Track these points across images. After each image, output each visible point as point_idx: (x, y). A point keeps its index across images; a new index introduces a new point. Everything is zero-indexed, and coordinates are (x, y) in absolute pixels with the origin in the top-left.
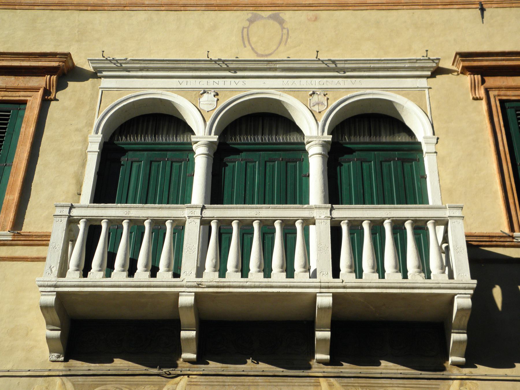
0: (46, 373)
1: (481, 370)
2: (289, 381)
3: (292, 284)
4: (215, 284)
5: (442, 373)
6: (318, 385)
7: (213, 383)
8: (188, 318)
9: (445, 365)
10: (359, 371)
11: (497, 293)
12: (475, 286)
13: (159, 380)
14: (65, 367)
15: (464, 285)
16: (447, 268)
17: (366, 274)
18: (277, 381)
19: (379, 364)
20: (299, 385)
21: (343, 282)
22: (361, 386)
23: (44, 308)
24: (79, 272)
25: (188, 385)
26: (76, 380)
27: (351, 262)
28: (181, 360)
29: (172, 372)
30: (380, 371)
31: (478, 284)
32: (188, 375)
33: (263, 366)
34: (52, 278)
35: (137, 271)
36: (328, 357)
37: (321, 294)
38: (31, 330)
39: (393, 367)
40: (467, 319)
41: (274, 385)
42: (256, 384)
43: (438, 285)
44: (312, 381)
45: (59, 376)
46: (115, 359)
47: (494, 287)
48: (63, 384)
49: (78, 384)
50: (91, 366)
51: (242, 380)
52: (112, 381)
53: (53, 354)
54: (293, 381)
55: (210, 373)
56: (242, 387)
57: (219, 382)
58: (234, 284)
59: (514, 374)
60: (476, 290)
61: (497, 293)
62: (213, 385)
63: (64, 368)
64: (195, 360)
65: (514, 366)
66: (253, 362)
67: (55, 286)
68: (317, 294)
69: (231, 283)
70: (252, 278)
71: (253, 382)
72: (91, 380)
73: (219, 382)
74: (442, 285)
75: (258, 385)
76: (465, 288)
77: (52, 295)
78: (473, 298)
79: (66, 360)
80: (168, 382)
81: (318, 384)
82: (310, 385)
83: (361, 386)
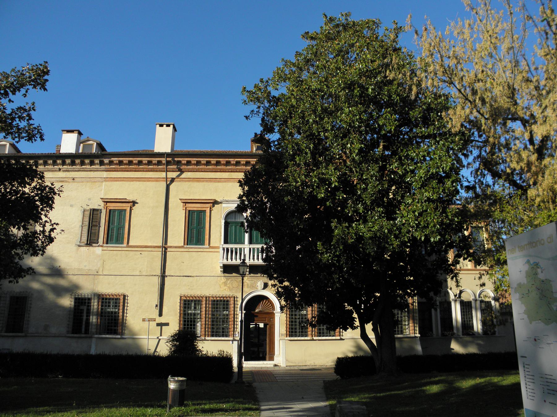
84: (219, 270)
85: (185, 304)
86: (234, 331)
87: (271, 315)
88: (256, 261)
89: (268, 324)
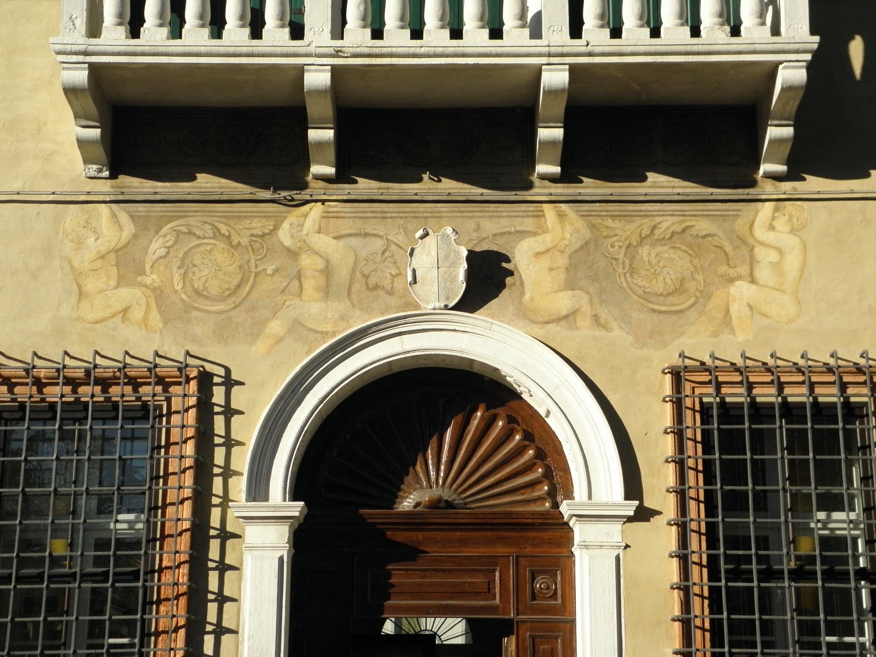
0: (83, 198)
1: (813, 184)
2: (492, 209)
3: (499, 50)
4: (366, 51)
5: (747, 191)
6: (541, 215)
7: (365, 215)
8: (320, 108)
10: (609, 191)
11: (856, 49)
12: (816, 46)
13: (275, 209)
14: (112, 187)
15: (797, 46)
16: (771, 8)
17: (628, 30)
18: (474, 209)
19: (644, 179)
20: (509, 217)
21: (588, 45)
22: (611, 216)
23: (71, 92)
24: (123, 28)
26: (135, 209)
27: (604, 7)
28: (311, 176)
29: (295, 197)
30: (644, 191)
31: (821, 44)
32: (323, 202)
33: (449, 186)
34: (78, 38)
35: (227, 27)
36: (557, 169)
37: (549, 67)
38: (45, 124)
39: (665, 184)
40: (797, 103)
41: (467, 217)
42: (436, 215)
43: (751, 47)
44: (531, 209)
46: (197, 175)
47: (853, 38)
48: (114, 215)
49: (139, 216)
50: (157, 187)
51: (414, 210)
52: (196, 211)
53: (90, 166)
54: (499, 209)
55: (360, 197)
56: (413, 220)
57: (375, 212)
58: (399, 50)
59: (865, 188)
60: (816, 54)
61: (856, 49)
62: (365, 218)
63: (111, 190)
64: (334, 177)
65: (868, 175)
66: (431, 178)
67: (86, 53)
68: (543, 67)
69: (394, 50)
70: (429, 39)
71: (433, 212)
72: (159, 209)
73: (375, 212)
74: (759, 47)
75: (441, 217)
76: (797, 52)
77: (81, 69)
78: (811, 67)
79: (113, 176)
80: (290, 212)
81: (541, 213)
82: (528, 216)
83: (611, 216)
84: (64, 141)
85: (731, 442)
87: (543, 541)
89: (507, 627)
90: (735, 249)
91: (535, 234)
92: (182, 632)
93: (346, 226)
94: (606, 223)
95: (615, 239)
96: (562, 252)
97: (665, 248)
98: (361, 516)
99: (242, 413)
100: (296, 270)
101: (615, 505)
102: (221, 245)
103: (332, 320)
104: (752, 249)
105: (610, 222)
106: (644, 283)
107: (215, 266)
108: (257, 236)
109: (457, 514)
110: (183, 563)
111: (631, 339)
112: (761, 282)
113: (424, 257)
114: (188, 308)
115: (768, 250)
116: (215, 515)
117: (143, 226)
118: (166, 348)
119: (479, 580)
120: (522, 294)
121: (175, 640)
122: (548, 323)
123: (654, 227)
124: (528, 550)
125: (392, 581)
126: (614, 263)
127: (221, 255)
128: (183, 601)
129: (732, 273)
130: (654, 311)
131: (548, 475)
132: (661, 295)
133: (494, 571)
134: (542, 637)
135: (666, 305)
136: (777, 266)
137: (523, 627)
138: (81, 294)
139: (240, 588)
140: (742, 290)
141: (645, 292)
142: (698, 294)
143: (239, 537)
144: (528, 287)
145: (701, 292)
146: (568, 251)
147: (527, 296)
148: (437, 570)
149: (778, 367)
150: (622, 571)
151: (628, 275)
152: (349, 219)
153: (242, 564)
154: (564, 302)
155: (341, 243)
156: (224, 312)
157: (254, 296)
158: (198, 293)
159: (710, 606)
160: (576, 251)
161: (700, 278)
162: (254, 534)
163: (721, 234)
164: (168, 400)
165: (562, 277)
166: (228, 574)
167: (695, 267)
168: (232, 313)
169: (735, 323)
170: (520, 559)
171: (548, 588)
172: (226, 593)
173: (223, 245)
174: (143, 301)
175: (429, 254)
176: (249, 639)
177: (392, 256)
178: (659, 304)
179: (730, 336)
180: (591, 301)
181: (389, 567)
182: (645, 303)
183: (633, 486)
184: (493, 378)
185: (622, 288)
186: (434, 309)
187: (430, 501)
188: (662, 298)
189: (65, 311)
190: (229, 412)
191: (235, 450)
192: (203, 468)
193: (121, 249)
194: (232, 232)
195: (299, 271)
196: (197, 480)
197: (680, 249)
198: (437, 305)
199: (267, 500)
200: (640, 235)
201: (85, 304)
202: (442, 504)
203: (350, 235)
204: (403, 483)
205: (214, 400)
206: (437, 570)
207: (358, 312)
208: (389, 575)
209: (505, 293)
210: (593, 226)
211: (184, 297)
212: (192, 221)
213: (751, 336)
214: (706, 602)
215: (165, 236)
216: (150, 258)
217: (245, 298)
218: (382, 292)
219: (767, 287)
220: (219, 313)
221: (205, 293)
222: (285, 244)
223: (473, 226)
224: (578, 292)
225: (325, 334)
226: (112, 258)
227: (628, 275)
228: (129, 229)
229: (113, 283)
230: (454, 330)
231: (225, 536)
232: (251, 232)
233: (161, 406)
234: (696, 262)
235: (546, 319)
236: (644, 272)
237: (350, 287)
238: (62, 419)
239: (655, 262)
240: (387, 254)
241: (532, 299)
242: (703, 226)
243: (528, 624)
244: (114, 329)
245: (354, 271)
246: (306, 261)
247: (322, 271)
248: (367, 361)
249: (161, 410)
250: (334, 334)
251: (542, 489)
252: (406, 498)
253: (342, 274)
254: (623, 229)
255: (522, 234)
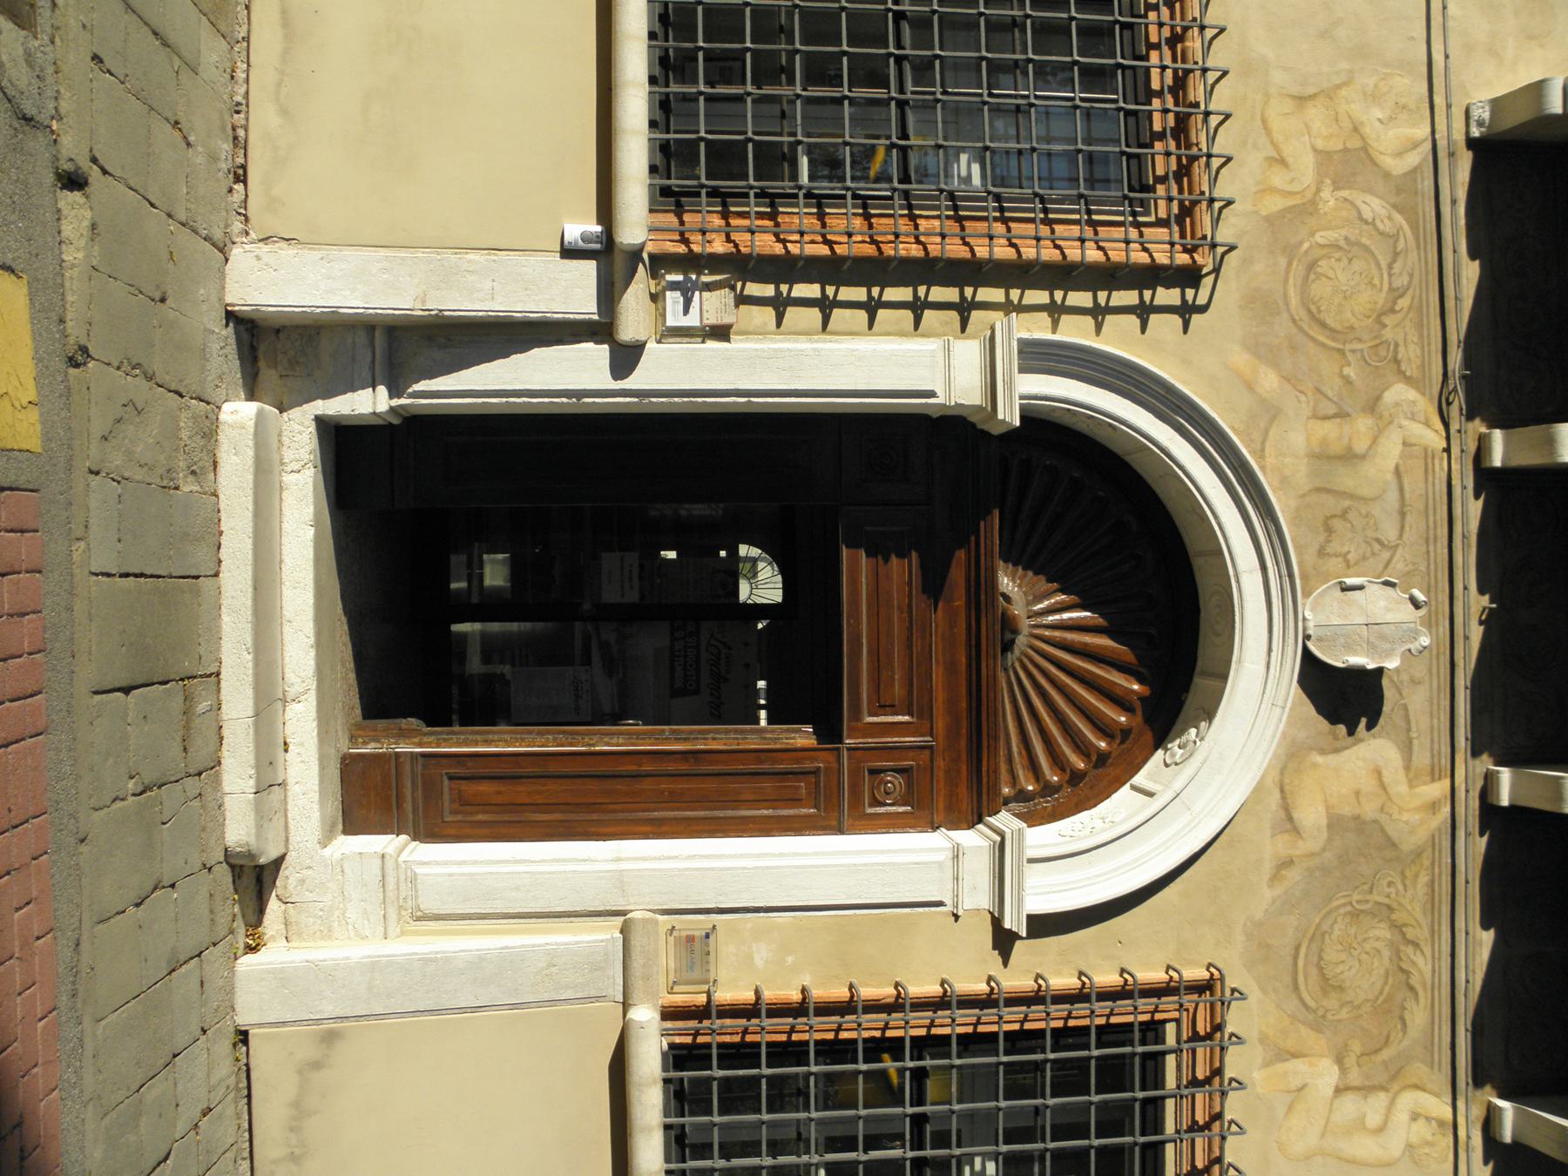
0: (1439, 100)
6: (1434, 776)
7: (1431, 512)
9: (1488, 1088)
19: (1485, 926)
20: (1432, 728)
22: (1432, 881)
25: (1426, 450)
28: (1483, 430)
29: (1455, 409)
32: (1448, 450)
36: (1505, 801)
38: (1541, 46)
45: (1433, 132)
46: (1477, 263)
53: (1487, 108)
62: (1427, 512)
64: (1486, 464)
79: (1471, 143)
80: (1431, 399)
83: (1432, 881)
86: (741, 267)
88: (1027, 622)
90: (1385, 1064)
91: (1407, 768)
92: (824, 250)
93: (1414, 484)
94: (1423, 873)
95: (1400, 887)
96: (1382, 809)
97: (1386, 961)
98: (989, 512)
99: (1143, 330)
100: (1350, 410)
101: (1020, 901)
102: (1381, 299)
103: (1282, 465)
104: (1383, 1088)
105: (1424, 879)
106: (1337, 932)
107: (1349, 290)
108: (1396, 352)
109: (995, 657)
110: (925, 249)
111: (1259, 915)
112: (1338, 1101)
113: (1382, 603)
114: (1290, 251)
115: (1383, 1111)
116: (994, 294)
117: (1402, 186)
118: (1232, 220)
119: (898, 690)
120: (1323, 752)
121: (813, 242)
122: (1282, 791)
123: (1416, 945)
124: (940, 763)
125: (894, 560)
126: (1366, 887)
127: (1367, 299)
128: (870, 250)
129: (1351, 1060)
130: (1297, 948)
131: (1047, 789)
132: (1320, 958)
133: (910, 714)
134: (817, 784)
135: (1305, 965)
136: (1359, 1124)
137: (831, 757)
138: (1301, 100)
139: (889, 334)
140: (1325, 1075)
141: (1323, 935)
142: (1320, 1013)
143: (963, 329)
144: (1333, 760)
145: (1323, 1017)
146: (1383, 818)
147: (1319, 759)
148: (910, 629)
149: (1223, 1138)
150: (921, 910)
151: (1349, 908)
152: (1424, 488)
153: (923, 336)
154: (1311, 815)
155: (1390, 477)
156: (1287, 305)
157: (1312, 348)
158: (1311, 266)
159: (873, 1039)
160: (1383, 830)
161: (1344, 1014)
162: (968, 352)
163: (1406, 1043)
164: (1160, 223)
165: (1347, 810)
166: (908, 315)
167: (1359, 1007)
168: (1285, 315)
169: (1280, 1067)
170: (927, 752)
171: (887, 794)
172: (881, 313)
173: (1381, 302)
174: (1297, 187)
175: (1388, 610)
176: (815, 350)
177: (1373, 554)
178: (1306, 956)
179: (1259, 1061)
180: (1312, 854)
181: (914, 554)
182: (1309, 935)
183: (1044, 926)
184: (1185, 708)
185: (1330, 900)
186: (1304, 619)
187: (1015, 617)
188: (1315, 959)
189: (1277, 77)
190: (1143, 312)
191: (1089, 321)
192: (1064, 275)
193: (1368, 155)
194: (1399, 316)
195: (1348, 415)
196: (1048, 267)
197: (1386, 983)
198: (1311, 624)
199: (1022, 370)
200: (1405, 925)
201: (1288, 106)
202: (1008, 636)
203: (1401, 489)
204: (1036, 573)
205: (1160, 290)
206: (910, 629)
207: (1293, 503)
208: (902, 555)
209: (1323, 724)
210: (1419, 855)
211: (1306, 245)
212: (1413, 256)
213: (1259, 1090)
214: (877, 1034)
215: (1390, 218)
216: (1358, 198)
217: (1308, 336)
218: (1322, 539)
219: (1330, 1111)
220: (1285, 295)
221: (1312, 276)
222: (1386, 394)
223: (1418, 675)
224: (1325, 835)
225: (1260, 454)
226: (1355, 143)
227: (1349, 908)
228: (1398, 166)
229: (1320, 144)
230: (1270, 650)
231: (964, 309)
232: (1401, 343)
233: (1147, 214)
234: (1367, 1008)
235: (1287, 788)
236: (1353, 931)
237: (1328, 491)
238: (1133, 68)
239: (1367, 947)
240: (1377, 547)
241: (1315, 765)
242: (1418, 1017)
243: (835, 765)
244: (1255, 146)
245: (1351, 496)
246: (1363, 425)
247: (1350, 449)
248: (1223, 519)
249: (1142, 214)
250: (1263, 468)
251: (1028, 782)
252: (1013, 581)
253: (1346, 480)
254: (1414, 899)
255: (1407, 749)
